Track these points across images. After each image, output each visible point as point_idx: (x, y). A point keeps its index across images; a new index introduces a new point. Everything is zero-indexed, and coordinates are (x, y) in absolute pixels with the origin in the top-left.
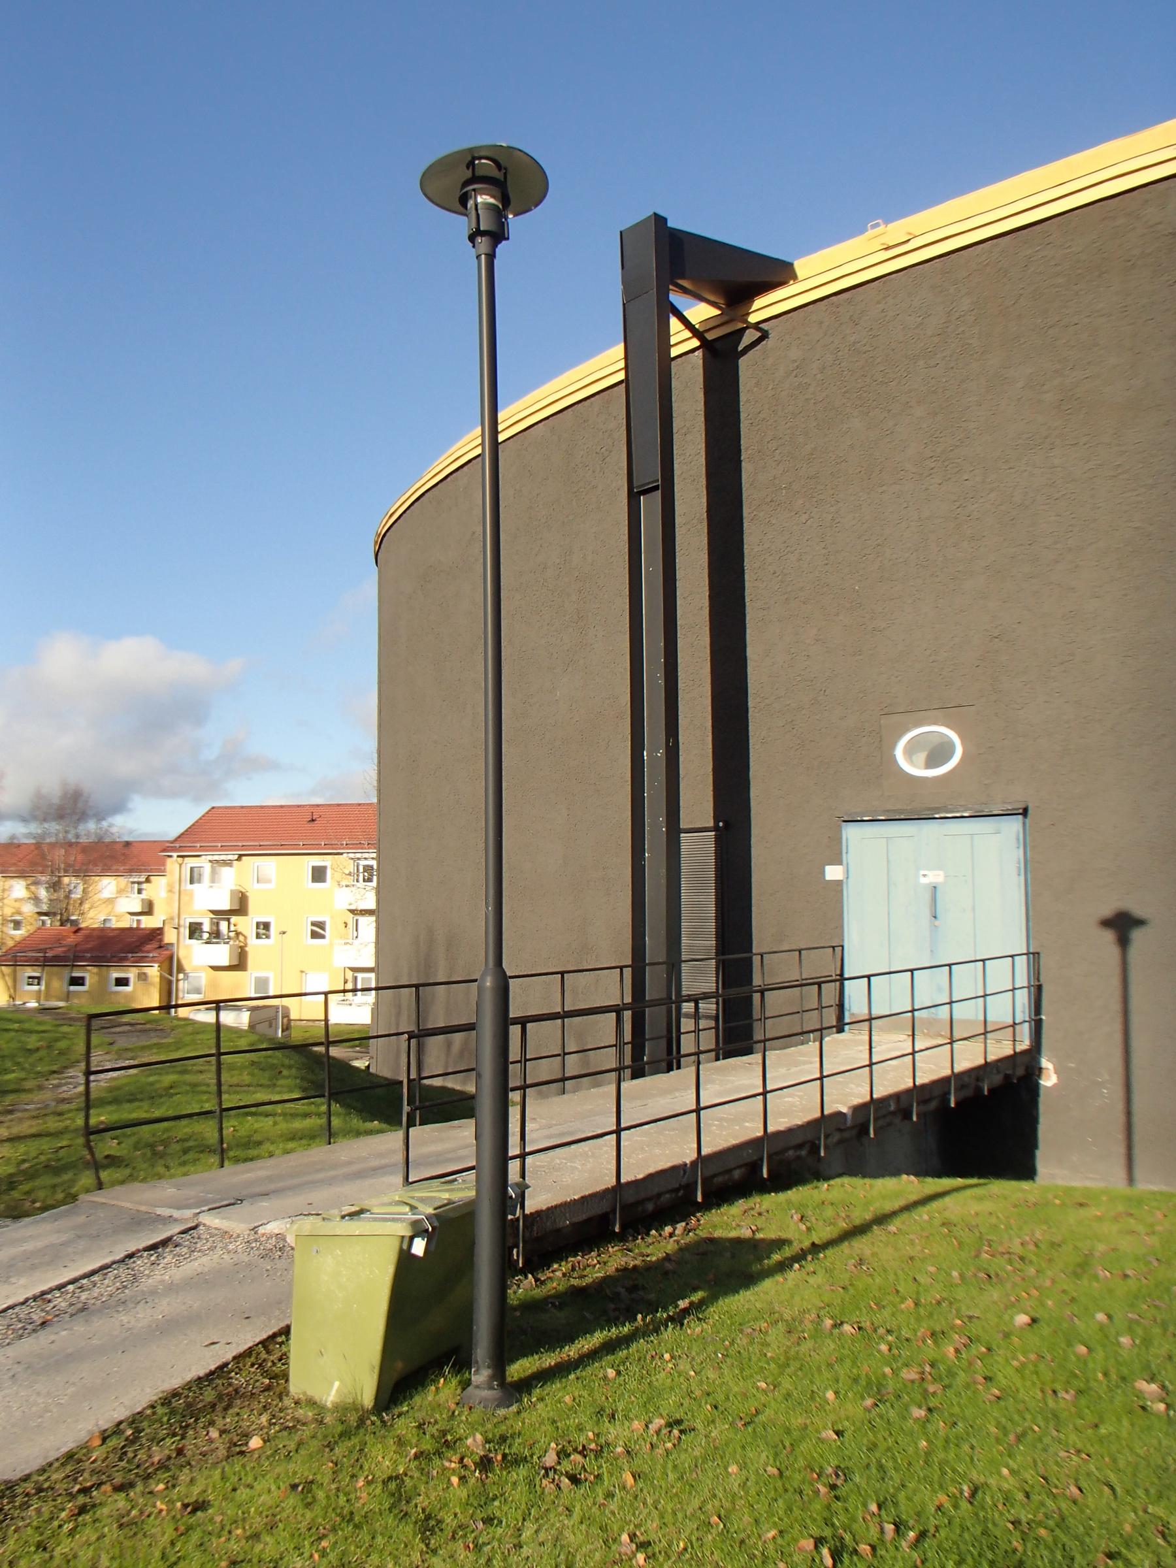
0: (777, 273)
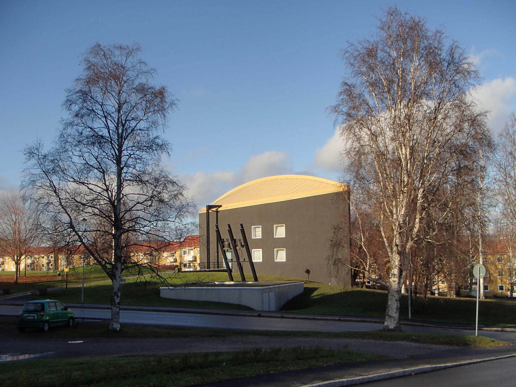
0: (220, 206)
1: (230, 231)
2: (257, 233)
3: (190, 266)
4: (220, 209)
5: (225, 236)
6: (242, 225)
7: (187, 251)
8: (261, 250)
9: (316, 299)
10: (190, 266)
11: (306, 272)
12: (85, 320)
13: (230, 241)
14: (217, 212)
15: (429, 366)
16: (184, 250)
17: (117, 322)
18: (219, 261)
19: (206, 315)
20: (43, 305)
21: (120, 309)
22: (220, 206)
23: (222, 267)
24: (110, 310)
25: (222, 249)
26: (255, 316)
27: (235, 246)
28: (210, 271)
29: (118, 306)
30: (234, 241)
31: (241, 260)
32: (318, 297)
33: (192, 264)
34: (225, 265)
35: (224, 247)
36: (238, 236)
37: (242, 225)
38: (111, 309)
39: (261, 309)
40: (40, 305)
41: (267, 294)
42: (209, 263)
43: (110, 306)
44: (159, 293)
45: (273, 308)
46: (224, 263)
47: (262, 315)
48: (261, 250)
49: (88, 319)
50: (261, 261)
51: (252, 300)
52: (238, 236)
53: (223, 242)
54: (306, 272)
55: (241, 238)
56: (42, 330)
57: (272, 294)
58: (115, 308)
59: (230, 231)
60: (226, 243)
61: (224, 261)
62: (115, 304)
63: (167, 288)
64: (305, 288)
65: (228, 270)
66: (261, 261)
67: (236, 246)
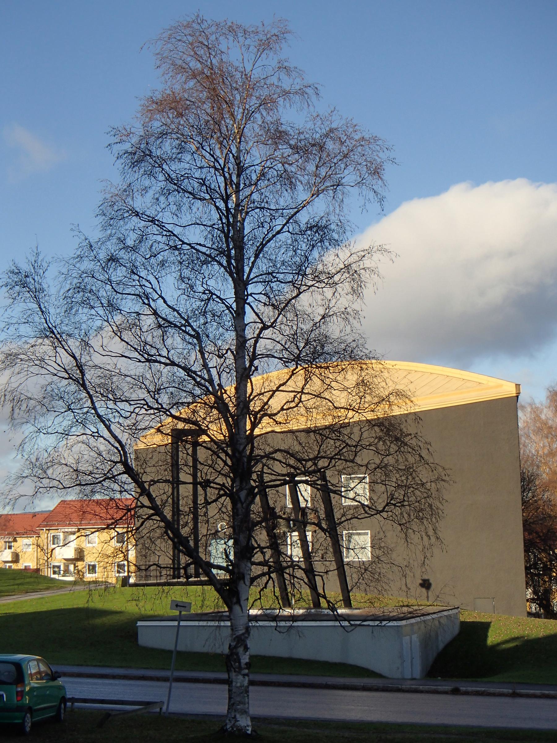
3: (67, 571)
7: (61, 536)
8: (369, 531)
9: (509, 649)
10: (67, 571)
11: (422, 585)
12: (76, 704)
16: (53, 533)
17: (245, 712)
19: (365, 694)
20: (18, 666)
21: (252, 683)
24: (226, 687)
26: (445, 693)
29: (246, 671)
32: (511, 645)
33: (72, 567)
38: (228, 682)
39: (400, 677)
40: (12, 668)
41: (408, 637)
43: (225, 676)
44: (136, 634)
45: (417, 672)
47: (463, 689)
48: (369, 531)
49: (85, 701)
51: (363, 651)
54: (422, 585)
56: (19, 729)
57: (415, 637)
58: (240, 677)
62: (240, 668)
63: (337, 624)
64: (464, 624)
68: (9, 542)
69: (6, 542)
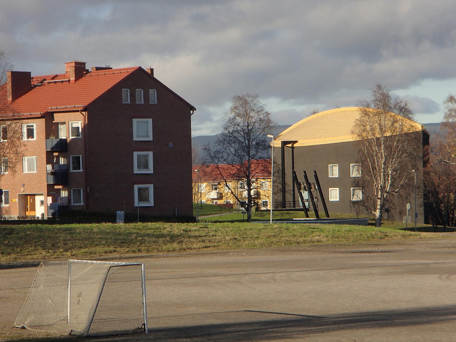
0: (296, 142)
1: (306, 177)
2: (334, 172)
4: (295, 145)
5: (301, 179)
6: (315, 172)
8: (338, 189)
13: (305, 185)
14: (293, 148)
15: (381, 262)
18: (296, 200)
22: (296, 142)
23: (299, 206)
25: (299, 191)
27: (310, 189)
28: (285, 210)
30: (309, 184)
31: (315, 200)
34: (301, 205)
35: (300, 189)
36: (312, 180)
37: (315, 172)
42: (285, 202)
46: (301, 202)
48: (338, 189)
50: (338, 200)
52: (312, 180)
53: (299, 185)
55: (315, 181)
59: (306, 177)
60: (302, 186)
61: (300, 200)
65: (305, 210)
66: (338, 200)
67: (311, 189)
68: (215, 185)
69: (213, 185)
